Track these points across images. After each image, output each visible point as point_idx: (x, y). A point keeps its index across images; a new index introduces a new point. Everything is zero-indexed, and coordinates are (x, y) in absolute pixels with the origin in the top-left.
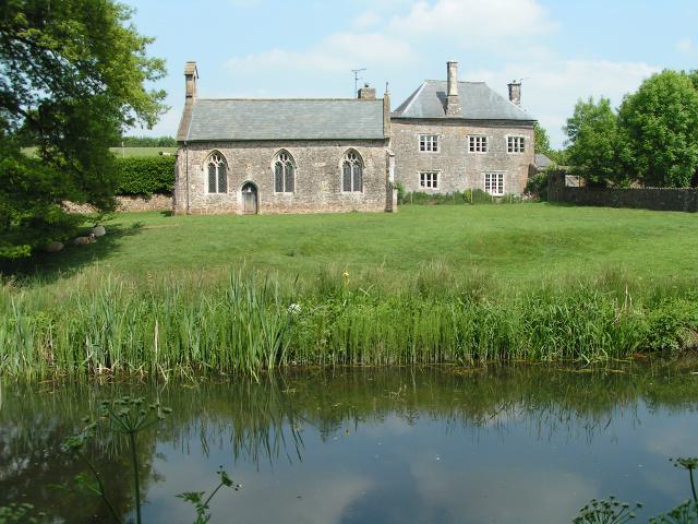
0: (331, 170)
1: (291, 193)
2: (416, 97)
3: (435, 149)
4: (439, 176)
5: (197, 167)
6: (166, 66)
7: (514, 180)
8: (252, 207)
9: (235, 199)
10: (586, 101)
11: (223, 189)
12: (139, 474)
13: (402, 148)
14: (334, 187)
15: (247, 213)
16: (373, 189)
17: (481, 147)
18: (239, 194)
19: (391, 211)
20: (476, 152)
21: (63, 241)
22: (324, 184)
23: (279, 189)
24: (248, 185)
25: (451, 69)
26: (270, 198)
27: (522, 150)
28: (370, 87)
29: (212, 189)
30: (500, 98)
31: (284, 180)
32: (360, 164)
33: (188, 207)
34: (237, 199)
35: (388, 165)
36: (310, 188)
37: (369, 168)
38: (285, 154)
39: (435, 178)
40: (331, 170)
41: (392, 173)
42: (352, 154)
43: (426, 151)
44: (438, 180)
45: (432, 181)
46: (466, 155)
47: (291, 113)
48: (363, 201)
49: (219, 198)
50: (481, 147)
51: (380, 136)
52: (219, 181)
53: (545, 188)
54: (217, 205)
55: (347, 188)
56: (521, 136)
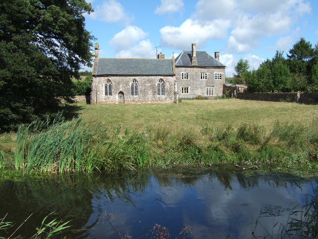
0: (153, 87)
1: (137, 96)
2: (180, 58)
4: (189, 88)
6: (193, 43)
7: (218, 91)
8: (122, 100)
11: (111, 94)
14: (154, 93)
15: (120, 103)
16: (169, 94)
18: (117, 96)
19: (176, 103)
21: (53, 191)
22: (150, 92)
23: (133, 95)
24: (121, 93)
25: (194, 46)
26: (129, 98)
27: (220, 78)
28: (163, 54)
29: (106, 94)
30: (212, 58)
31: (134, 91)
32: (163, 86)
34: (116, 98)
35: (175, 85)
36: (144, 93)
37: (167, 85)
38: (135, 80)
39: (188, 89)
40: (153, 87)
41: (176, 88)
44: (189, 90)
47: (136, 65)
48: (166, 100)
51: (172, 74)
52: (109, 91)
53: (229, 92)
55: (159, 94)
56: (220, 73)
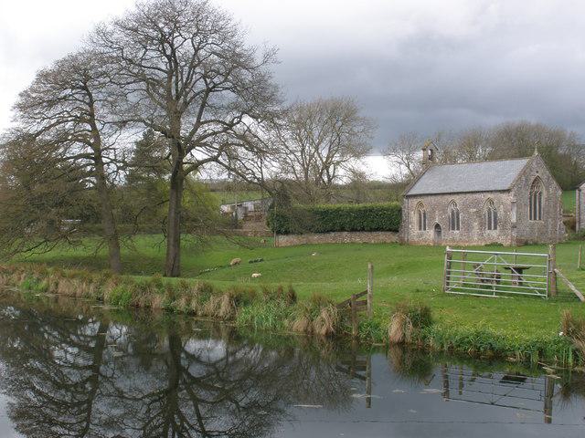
14: (481, 225)
29: (420, 229)
36: (469, 228)
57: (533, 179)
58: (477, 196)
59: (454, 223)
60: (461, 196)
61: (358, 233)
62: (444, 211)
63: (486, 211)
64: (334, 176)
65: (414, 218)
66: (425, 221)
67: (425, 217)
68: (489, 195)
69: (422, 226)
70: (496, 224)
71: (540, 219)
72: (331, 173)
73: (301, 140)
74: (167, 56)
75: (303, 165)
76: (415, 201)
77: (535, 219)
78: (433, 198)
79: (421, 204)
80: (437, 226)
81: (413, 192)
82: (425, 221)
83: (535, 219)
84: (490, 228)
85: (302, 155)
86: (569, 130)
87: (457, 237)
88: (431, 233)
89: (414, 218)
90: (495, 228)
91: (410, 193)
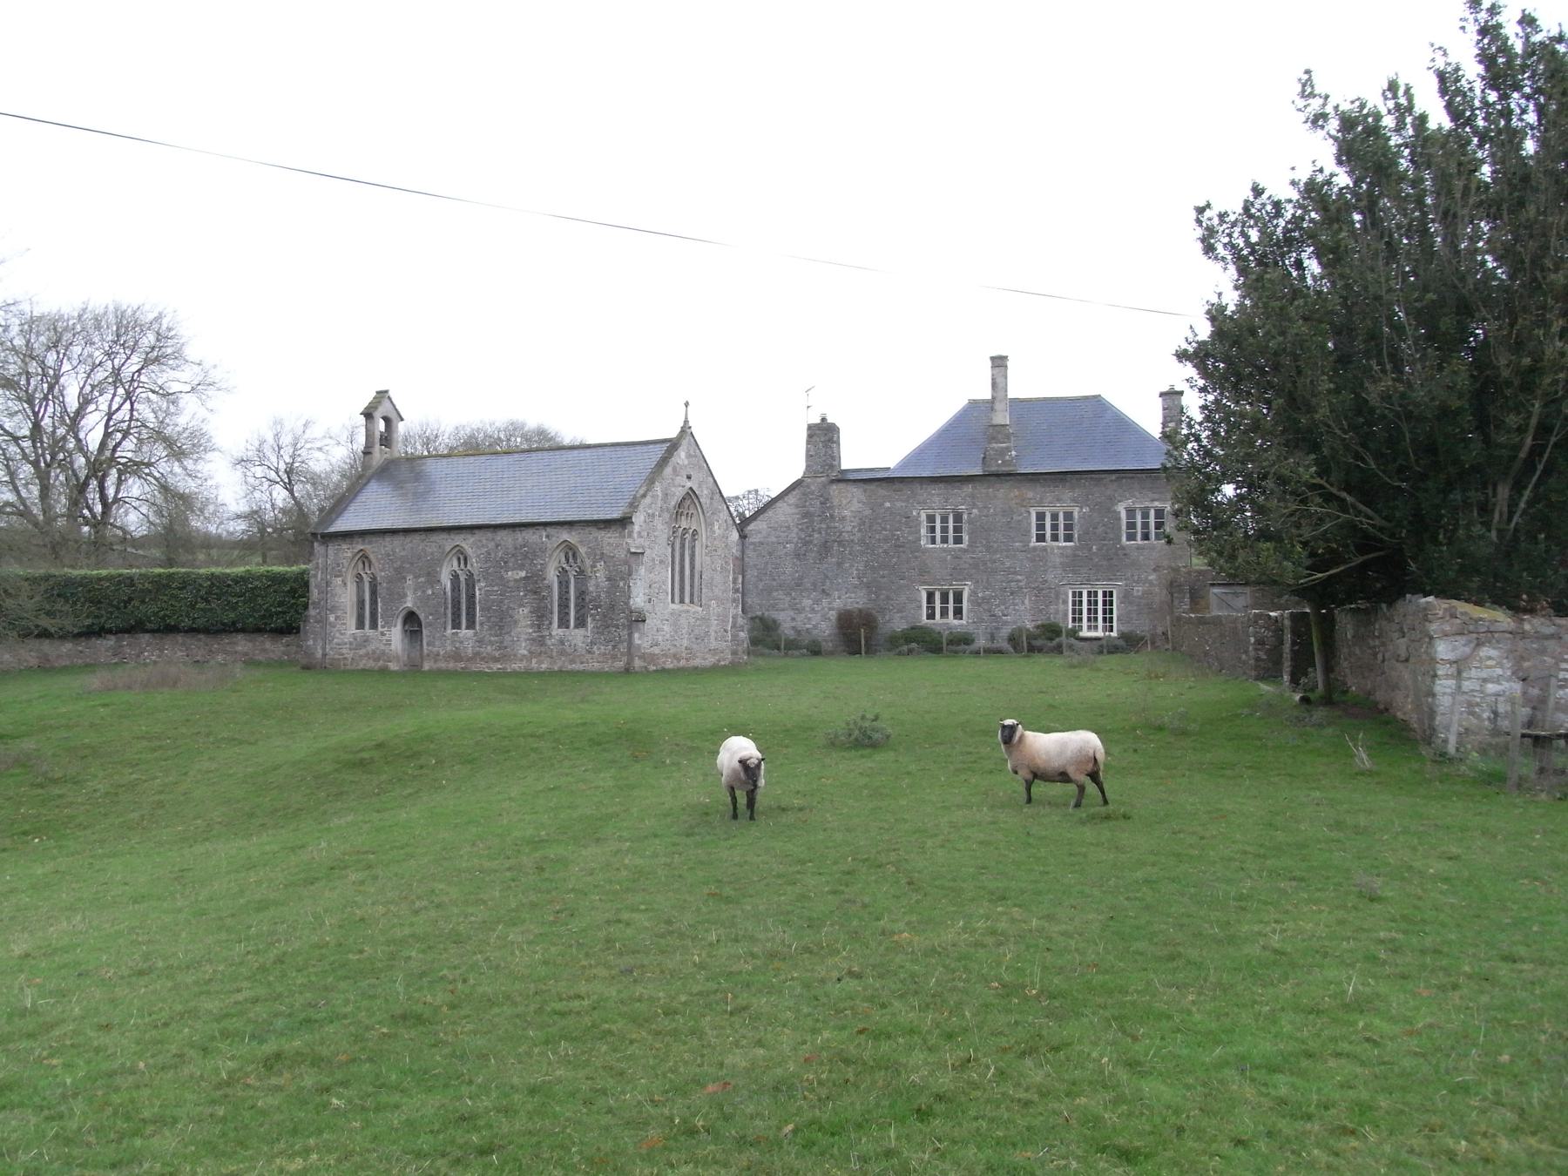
3: (958, 540)
5: (339, 581)
6: (1223, 211)
9: (388, 643)
10: (1207, 307)
11: (374, 625)
12: (1482, 770)
13: (886, 540)
14: (541, 616)
17: (1061, 532)
20: (1049, 542)
22: (523, 614)
29: (360, 625)
33: (324, 655)
36: (502, 622)
42: (570, 551)
43: (1049, 542)
45: (951, 606)
46: (1026, 549)
49: (366, 640)
50: (1061, 532)
54: (362, 652)
57: (679, 493)
58: (530, 536)
59: (461, 608)
60: (479, 535)
61: (180, 638)
62: (433, 578)
63: (552, 576)
64: (116, 500)
65: (346, 596)
66: (374, 602)
67: (374, 593)
68: (565, 535)
69: (368, 616)
70: (581, 606)
71: (692, 602)
72: (111, 492)
73: (30, 401)
74: (30, 462)
75: (35, 464)
76: (347, 551)
77: (682, 601)
78: (398, 541)
79: (364, 559)
80: (411, 618)
81: (341, 525)
82: (374, 602)
83: (682, 601)
84: (456, 625)
85: (34, 446)
86: (150, 655)
87: (469, 648)
88: (395, 636)
89: (346, 596)
90: (581, 623)
91: (332, 529)
